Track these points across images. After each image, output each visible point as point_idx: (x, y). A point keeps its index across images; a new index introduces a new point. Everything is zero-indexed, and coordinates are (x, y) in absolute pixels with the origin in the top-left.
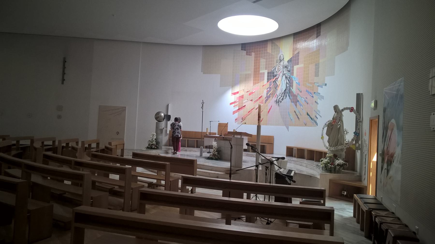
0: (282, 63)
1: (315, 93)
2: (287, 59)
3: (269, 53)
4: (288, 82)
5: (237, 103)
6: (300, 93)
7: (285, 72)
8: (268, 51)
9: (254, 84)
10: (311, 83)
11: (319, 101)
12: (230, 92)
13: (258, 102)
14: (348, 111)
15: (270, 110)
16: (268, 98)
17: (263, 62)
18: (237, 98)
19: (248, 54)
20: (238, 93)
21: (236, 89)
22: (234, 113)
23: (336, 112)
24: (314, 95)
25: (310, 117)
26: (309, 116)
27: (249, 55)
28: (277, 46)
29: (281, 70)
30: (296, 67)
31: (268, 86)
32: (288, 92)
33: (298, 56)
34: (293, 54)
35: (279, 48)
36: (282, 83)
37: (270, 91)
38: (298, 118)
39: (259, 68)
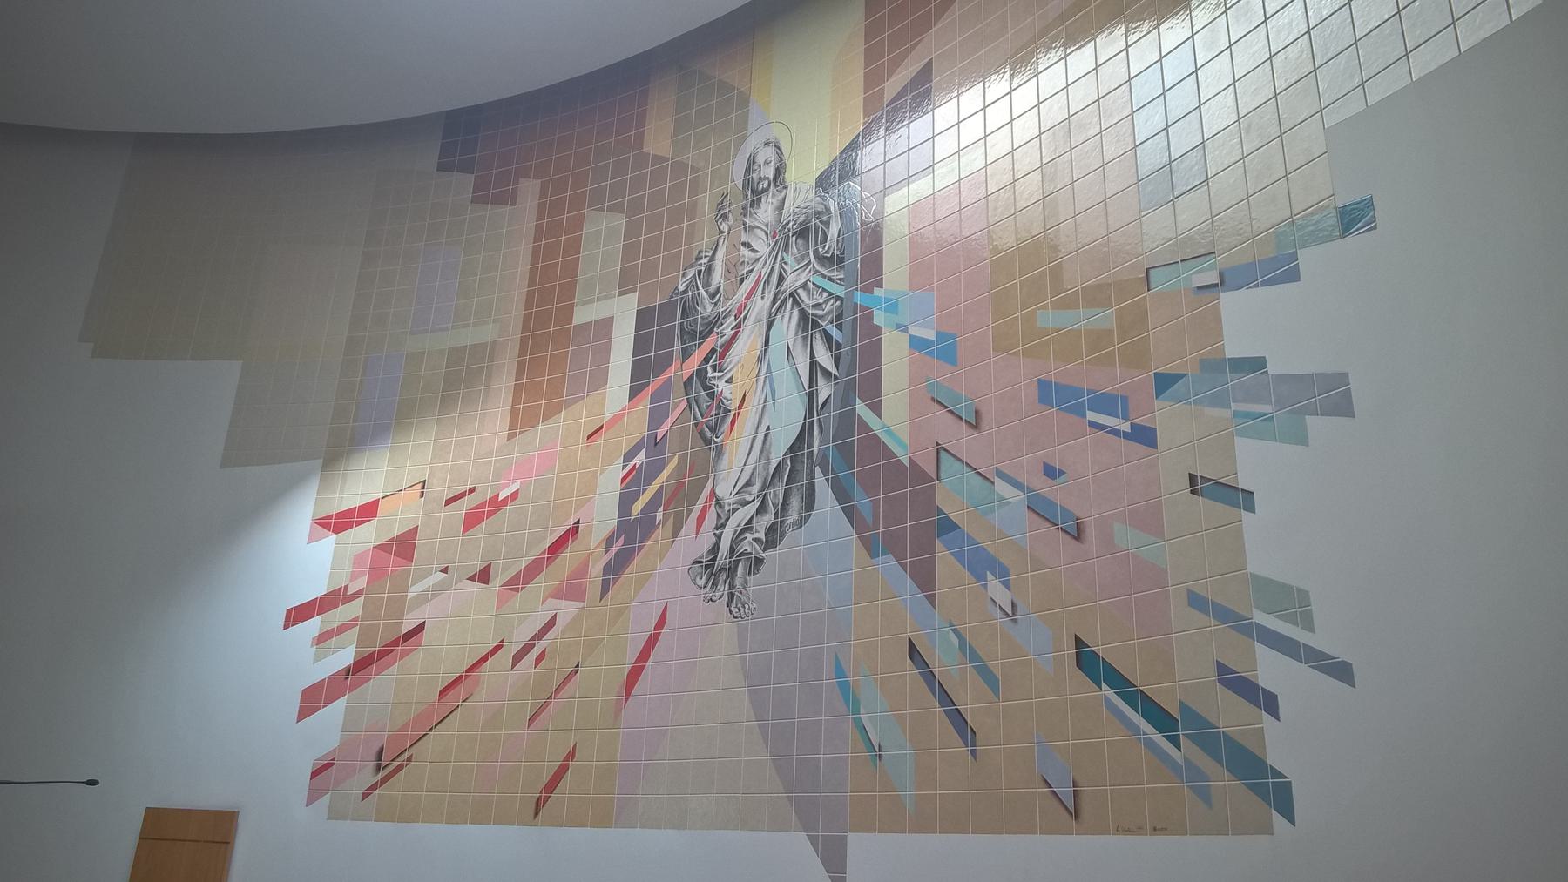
0: (766, 212)
1: (1164, 383)
3: (658, 159)
4: (825, 358)
5: (355, 609)
7: (791, 282)
9: (520, 422)
11: (1255, 462)
12: (304, 509)
13: (541, 583)
15: (644, 656)
16: (631, 535)
17: (603, 235)
18: (358, 559)
19: (495, 192)
21: (365, 480)
22: (313, 699)
24: (1164, 415)
25: (1135, 697)
26: (1116, 679)
27: (500, 200)
31: (636, 427)
32: (834, 450)
35: (744, 101)
36: (767, 387)
37: (653, 469)
38: (958, 720)
39: (569, 291)
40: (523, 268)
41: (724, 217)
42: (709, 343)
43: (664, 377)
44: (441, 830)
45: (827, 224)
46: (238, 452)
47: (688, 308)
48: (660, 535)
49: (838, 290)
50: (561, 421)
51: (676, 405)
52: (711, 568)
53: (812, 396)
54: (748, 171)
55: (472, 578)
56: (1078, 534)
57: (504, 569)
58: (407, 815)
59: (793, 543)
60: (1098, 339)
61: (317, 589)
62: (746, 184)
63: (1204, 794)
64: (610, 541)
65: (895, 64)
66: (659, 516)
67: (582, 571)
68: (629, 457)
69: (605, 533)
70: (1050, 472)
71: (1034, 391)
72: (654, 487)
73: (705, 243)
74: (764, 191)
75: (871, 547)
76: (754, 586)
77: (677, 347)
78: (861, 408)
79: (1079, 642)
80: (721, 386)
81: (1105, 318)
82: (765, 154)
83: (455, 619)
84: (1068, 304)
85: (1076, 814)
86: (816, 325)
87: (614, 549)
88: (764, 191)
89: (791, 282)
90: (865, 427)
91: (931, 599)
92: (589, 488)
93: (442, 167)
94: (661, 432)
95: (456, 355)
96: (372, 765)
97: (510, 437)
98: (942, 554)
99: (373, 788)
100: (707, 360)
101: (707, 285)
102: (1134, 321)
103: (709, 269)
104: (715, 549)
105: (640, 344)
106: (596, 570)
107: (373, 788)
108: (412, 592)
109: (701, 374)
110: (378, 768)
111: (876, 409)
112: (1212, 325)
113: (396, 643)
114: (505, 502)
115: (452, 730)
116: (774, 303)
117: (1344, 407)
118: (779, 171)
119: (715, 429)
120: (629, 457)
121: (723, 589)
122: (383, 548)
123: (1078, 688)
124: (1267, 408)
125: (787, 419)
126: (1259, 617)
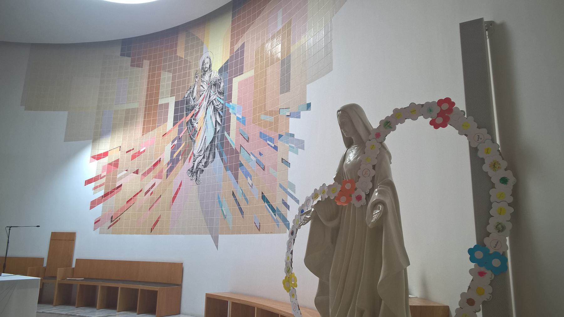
0: (206, 78)
1: (280, 136)
2: (217, 65)
3: (181, 58)
5: (103, 180)
6: (245, 144)
7: (212, 98)
8: (179, 54)
9: (145, 131)
10: (271, 113)
11: (291, 157)
12: (88, 153)
13: (151, 174)
14: (423, 122)
15: (176, 193)
16: (174, 162)
17: (166, 78)
19: (136, 63)
20: (106, 154)
21: (104, 146)
22: (93, 204)
23: (349, 143)
24: (279, 144)
26: (268, 202)
28: (198, 39)
29: (205, 93)
30: (236, 81)
31: (174, 134)
32: (219, 144)
33: (243, 52)
34: (232, 50)
36: (206, 125)
37: (179, 145)
38: (241, 209)
39: (157, 94)
40: (145, 87)
41: (197, 77)
42: (193, 112)
43: (182, 121)
44: (128, 236)
45: (220, 83)
46: (68, 138)
47: (188, 103)
48: (180, 162)
49: (222, 102)
54: (203, 65)
55: (134, 173)
58: (119, 232)
59: (211, 166)
60: (271, 124)
61: (93, 175)
62: (203, 68)
63: (278, 225)
64: (168, 164)
65: (238, 40)
66: (180, 158)
67: (161, 171)
68: (173, 142)
69: (167, 162)
70: (261, 154)
72: (179, 150)
73: (192, 84)
75: (226, 168)
76: (202, 177)
77: (185, 113)
78: (226, 133)
79: (262, 193)
80: (195, 125)
82: (207, 60)
83: (130, 183)
84: (266, 114)
85: (259, 230)
87: (169, 166)
89: (212, 98)
90: (226, 139)
91: (237, 182)
92: (163, 150)
93: (122, 55)
95: (128, 111)
97: (143, 135)
98: (240, 171)
99: (111, 226)
100: (192, 117)
101: (192, 96)
102: (277, 120)
103: (193, 91)
104: (193, 167)
105: (176, 111)
106: (165, 171)
107: (111, 226)
109: (191, 120)
110: (112, 221)
111: (229, 134)
113: (114, 189)
114: (142, 153)
115: (130, 211)
117: (303, 148)
118: (210, 66)
119: (194, 135)
120: (173, 142)
121: (195, 177)
122: (110, 164)
124: (293, 146)
126: (289, 190)
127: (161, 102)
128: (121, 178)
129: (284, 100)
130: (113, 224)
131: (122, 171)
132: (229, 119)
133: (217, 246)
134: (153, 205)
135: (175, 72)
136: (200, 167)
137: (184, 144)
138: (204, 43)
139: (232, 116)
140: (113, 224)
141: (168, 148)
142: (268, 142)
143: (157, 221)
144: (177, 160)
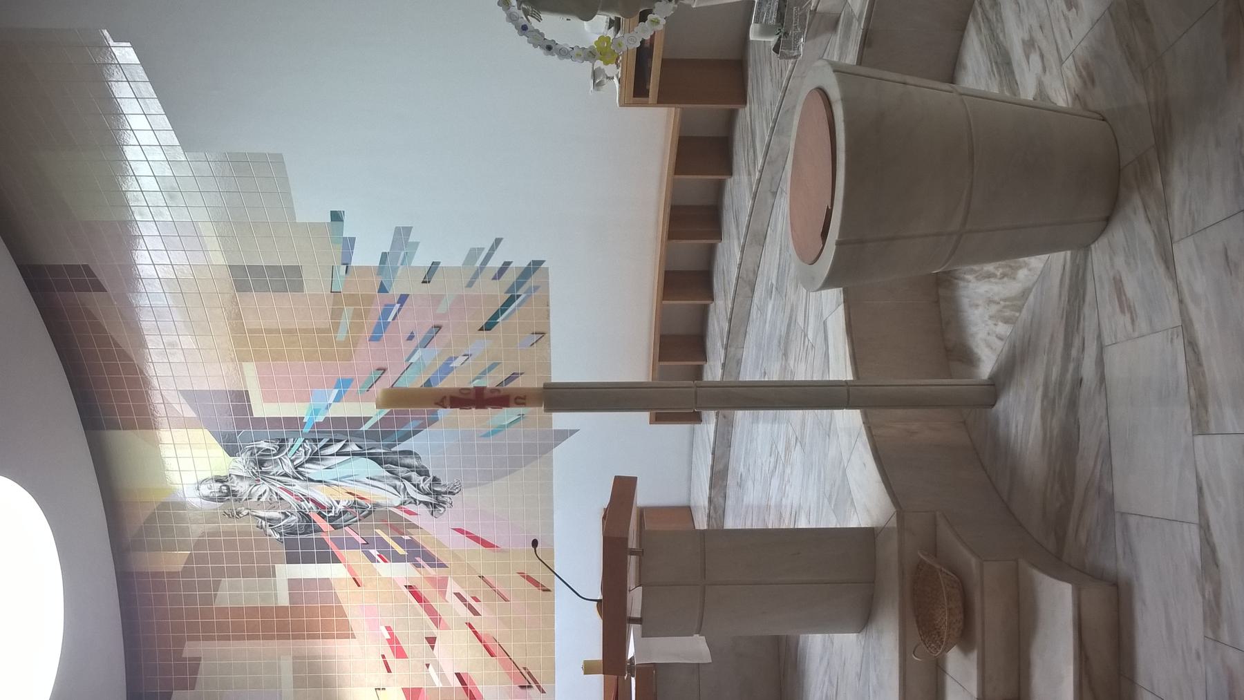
0: (242, 487)
1: (382, 289)
4: (335, 448)
7: (288, 468)
9: (346, 632)
10: (336, 314)
11: (422, 260)
13: (437, 605)
15: (476, 539)
16: (417, 554)
17: (234, 593)
24: (396, 291)
26: (496, 316)
27: (195, 669)
28: (151, 519)
31: (354, 557)
32: (383, 445)
36: (347, 480)
37: (382, 543)
39: (266, 611)
41: (238, 513)
43: (330, 543)
45: (259, 449)
47: (292, 531)
48: (418, 537)
50: (346, 606)
51: (347, 533)
52: (434, 506)
53: (354, 454)
55: (433, 647)
56: (439, 327)
57: (428, 628)
59: (427, 462)
60: (357, 315)
62: (221, 500)
63: (536, 288)
64: (418, 566)
66: (406, 537)
70: (411, 338)
71: (373, 343)
74: (228, 488)
78: (365, 428)
79: (481, 329)
80: (340, 507)
81: (348, 311)
82: (205, 490)
84: (336, 326)
86: (316, 453)
87: (422, 563)
88: (228, 488)
90: (375, 425)
92: (390, 581)
94: (361, 541)
95: (298, 682)
96: (528, 691)
99: (539, 687)
100: (324, 517)
101: (279, 520)
102: (352, 299)
103: (269, 520)
104: (426, 504)
105: (308, 559)
106: (433, 572)
107: (539, 687)
108: (438, 684)
109: (331, 520)
110: (530, 687)
111: (367, 419)
112: (364, 270)
113: (466, 689)
114: (391, 634)
115: (510, 646)
116: (297, 478)
117: (408, 230)
119: (363, 508)
120: (372, 559)
121: (447, 498)
123: (499, 330)
125: (366, 467)
126: (478, 264)
127: (284, 600)
128: (443, 677)
129: (315, 284)
130: (536, 682)
131: (429, 676)
132: (338, 421)
133: (573, 432)
134: (499, 594)
135: (220, 573)
136: (426, 487)
137: (379, 531)
138: (163, 499)
139: (331, 414)
140: (536, 682)
141: (386, 570)
142: (390, 319)
143: (529, 579)
144: (411, 545)
